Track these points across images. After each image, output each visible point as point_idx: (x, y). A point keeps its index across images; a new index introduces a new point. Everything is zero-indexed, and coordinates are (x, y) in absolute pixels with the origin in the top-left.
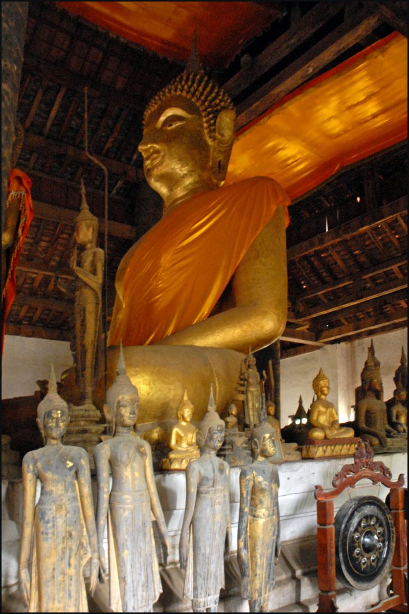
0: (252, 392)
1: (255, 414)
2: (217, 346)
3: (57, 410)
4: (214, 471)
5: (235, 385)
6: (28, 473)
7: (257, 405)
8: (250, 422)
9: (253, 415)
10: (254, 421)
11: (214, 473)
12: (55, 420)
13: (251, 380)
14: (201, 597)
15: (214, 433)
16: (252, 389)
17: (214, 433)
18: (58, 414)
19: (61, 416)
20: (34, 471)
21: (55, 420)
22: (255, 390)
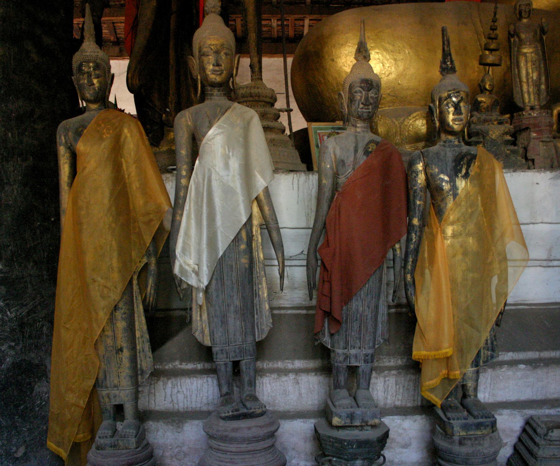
0: (525, 54)
1: (531, 90)
2: (548, 9)
3: (88, 62)
4: (356, 151)
5: (484, 41)
6: (60, 146)
7: (535, 76)
8: (523, 102)
9: (529, 92)
10: (529, 102)
11: (355, 155)
12: (86, 76)
13: (523, 36)
14: (339, 348)
15: (356, 92)
16: (525, 51)
17: (356, 92)
18: (90, 68)
19: (94, 69)
20: (66, 142)
21: (86, 76)
22: (531, 50)
